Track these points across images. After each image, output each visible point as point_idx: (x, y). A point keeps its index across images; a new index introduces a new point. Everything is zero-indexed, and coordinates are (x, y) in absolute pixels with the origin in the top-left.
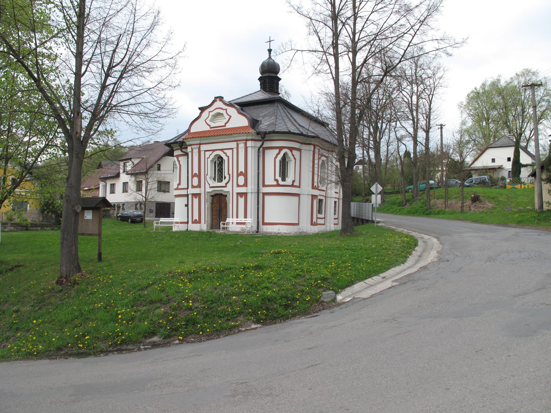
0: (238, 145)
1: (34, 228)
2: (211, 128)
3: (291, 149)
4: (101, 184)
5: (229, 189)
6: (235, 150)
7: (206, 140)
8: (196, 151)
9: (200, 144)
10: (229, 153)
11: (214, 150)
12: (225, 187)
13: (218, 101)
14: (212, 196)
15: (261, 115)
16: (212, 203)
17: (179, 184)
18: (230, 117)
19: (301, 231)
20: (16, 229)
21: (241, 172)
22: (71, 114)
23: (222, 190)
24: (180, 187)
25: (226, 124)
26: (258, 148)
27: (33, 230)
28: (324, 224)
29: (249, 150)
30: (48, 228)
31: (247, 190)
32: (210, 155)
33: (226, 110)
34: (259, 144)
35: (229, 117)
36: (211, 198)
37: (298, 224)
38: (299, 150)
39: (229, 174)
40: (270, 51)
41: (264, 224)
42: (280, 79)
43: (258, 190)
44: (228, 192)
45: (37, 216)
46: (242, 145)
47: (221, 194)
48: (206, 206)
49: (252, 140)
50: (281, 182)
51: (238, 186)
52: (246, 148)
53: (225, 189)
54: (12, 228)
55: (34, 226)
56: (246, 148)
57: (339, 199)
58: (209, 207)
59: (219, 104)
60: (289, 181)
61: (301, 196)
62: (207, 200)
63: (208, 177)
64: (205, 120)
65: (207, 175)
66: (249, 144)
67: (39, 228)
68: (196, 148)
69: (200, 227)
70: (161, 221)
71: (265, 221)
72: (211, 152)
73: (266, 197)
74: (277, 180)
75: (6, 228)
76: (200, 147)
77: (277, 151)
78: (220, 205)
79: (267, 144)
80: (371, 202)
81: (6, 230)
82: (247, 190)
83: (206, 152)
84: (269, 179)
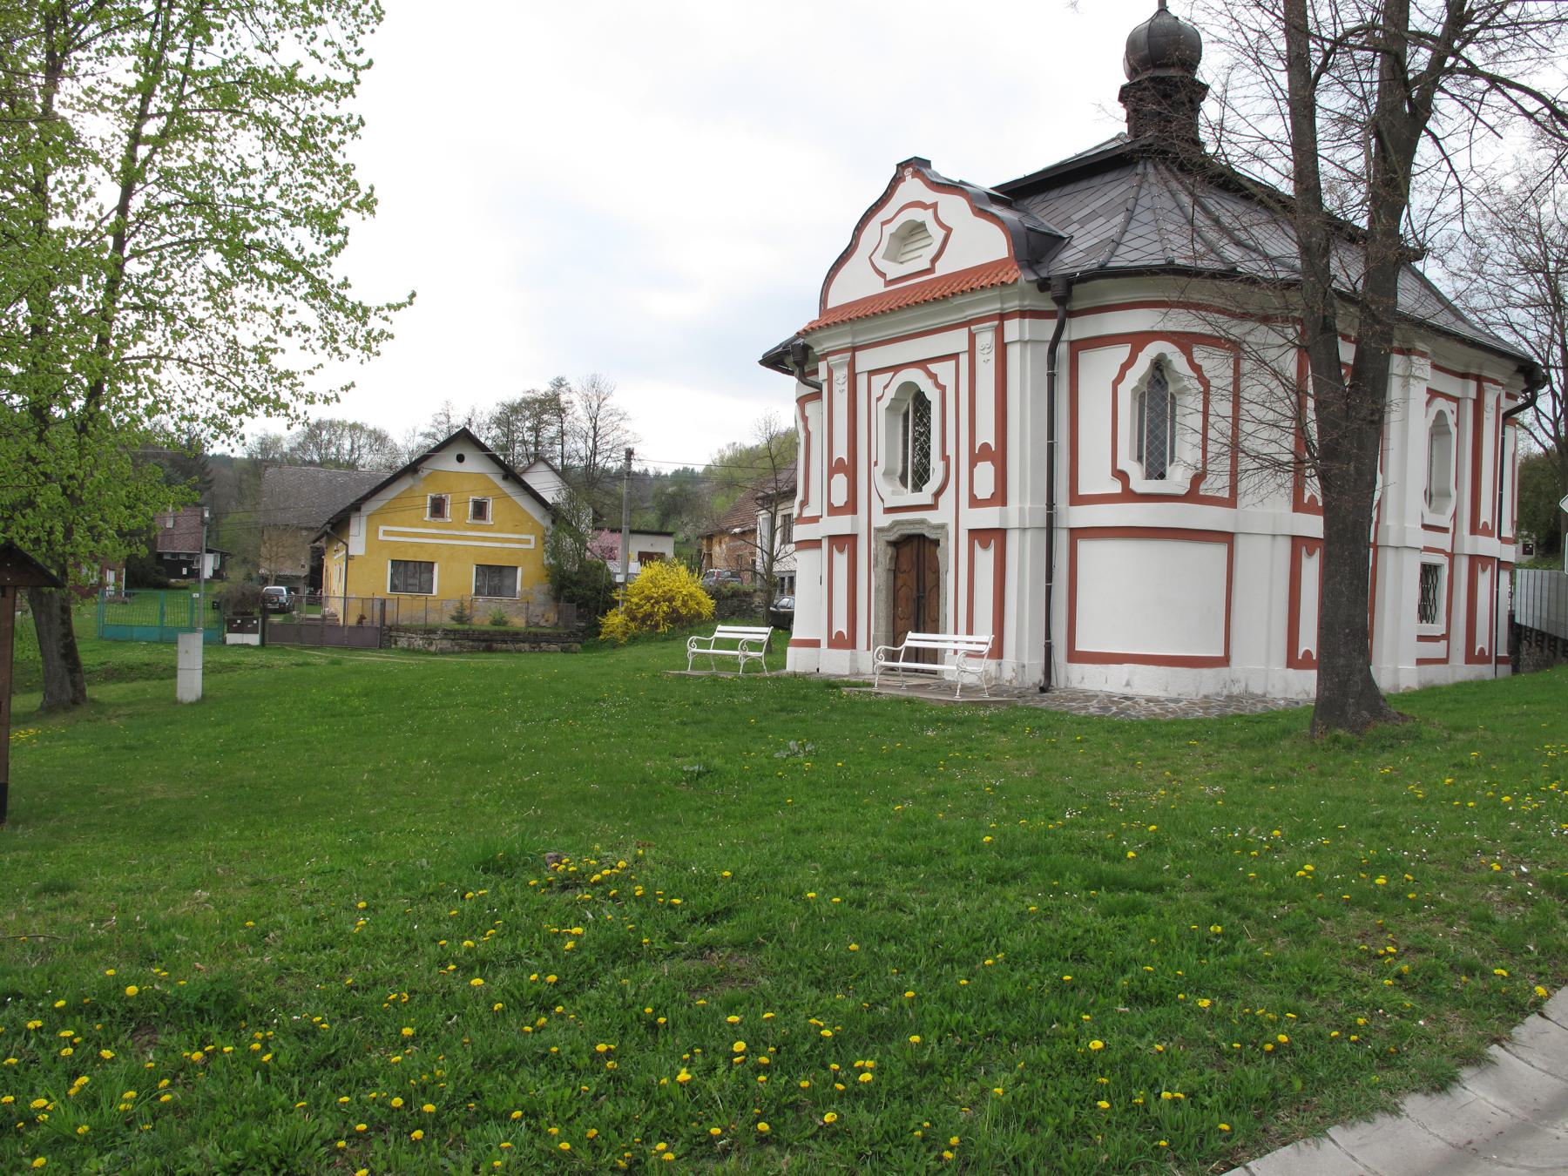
0: (972, 338)
1: (510, 646)
2: (889, 283)
3: (1185, 341)
4: (763, 516)
6: (964, 359)
8: (841, 375)
10: (944, 371)
11: (896, 369)
12: (932, 507)
13: (909, 178)
14: (890, 543)
15: (1075, 217)
16: (895, 571)
18: (949, 230)
19: (1236, 690)
20: (457, 648)
21: (985, 446)
22: (12, 191)
23: (922, 522)
25: (934, 260)
26: (1046, 348)
27: (507, 651)
28: (1445, 661)
29: (1014, 353)
30: (553, 647)
31: (1004, 517)
32: (886, 387)
33: (934, 206)
34: (1048, 327)
35: (943, 233)
36: (890, 551)
37: (1225, 661)
38: (1235, 347)
39: (945, 458)
41: (1074, 656)
43: (1050, 519)
44: (943, 527)
45: (542, 608)
46: (986, 339)
47: (922, 537)
49: (1023, 314)
50: (1139, 484)
51: (975, 502)
52: (1002, 349)
53: (932, 517)
54: (446, 644)
55: (534, 639)
56: (1002, 349)
57: (1452, 556)
58: (883, 587)
59: (912, 188)
60: (1177, 479)
61: (1241, 544)
62: (876, 559)
63: (878, 472)
65: (876, 464)
66: (1013, 329)
67: (526, 646)
68: (840, 366)
69: (853, 661)
70: (717, 635)
71: (1081, 646)
73: (1085, 548)
74: (1122, 476)
75: (431, 644)
76: (853, 358)
77: (1122, 352)
78: (920, 579)
79: (1079, 329)
81: (433, 648)
82: (1004, 517)
84: (1095, 477)
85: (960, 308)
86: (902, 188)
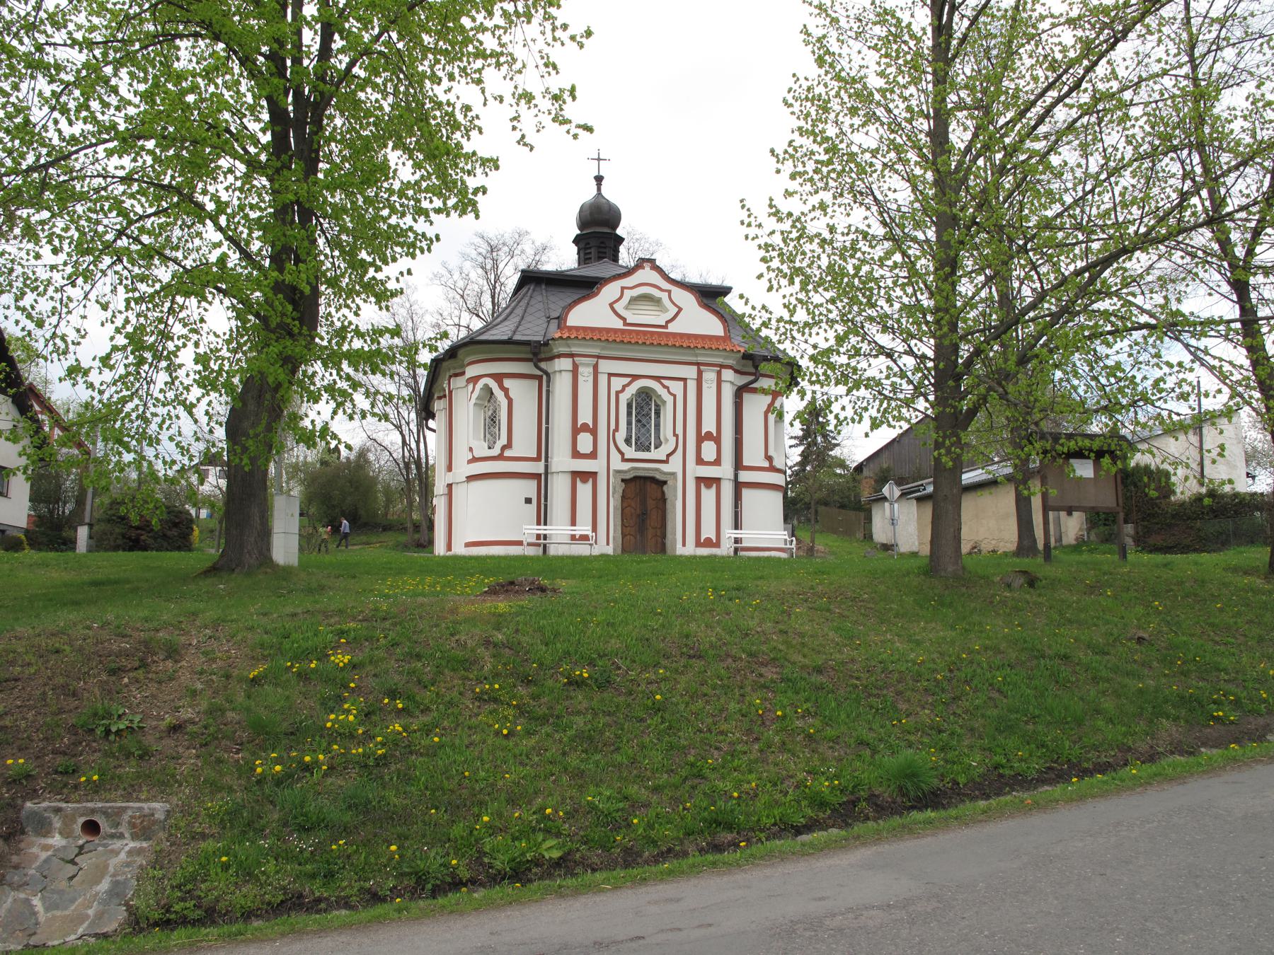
0: (700, 373)
5: (674, 466)
6: (692, 386)
7: (661, 353)
9: (599, 357)
10: (676, 387)
11: (635, 377)
12: (666, 462)
17: (508, 446)
18: (680, 310)
23: (657, 470)
24: (507, 453)
25: (667, 322)
33: (669, 292)
39: (676, 435)
40: (599, 179)
42: (620, 240)
44: (673, 474)
48: (609, 506)
51: (700, 461)
53: (664, 467)
64: (611, 305)
65: (617, 429)
68: (587, 365)
72: (628, 380)
80: (74, 549)
83: (613, 379)
85: (696, 355)
86: (640, 272)
